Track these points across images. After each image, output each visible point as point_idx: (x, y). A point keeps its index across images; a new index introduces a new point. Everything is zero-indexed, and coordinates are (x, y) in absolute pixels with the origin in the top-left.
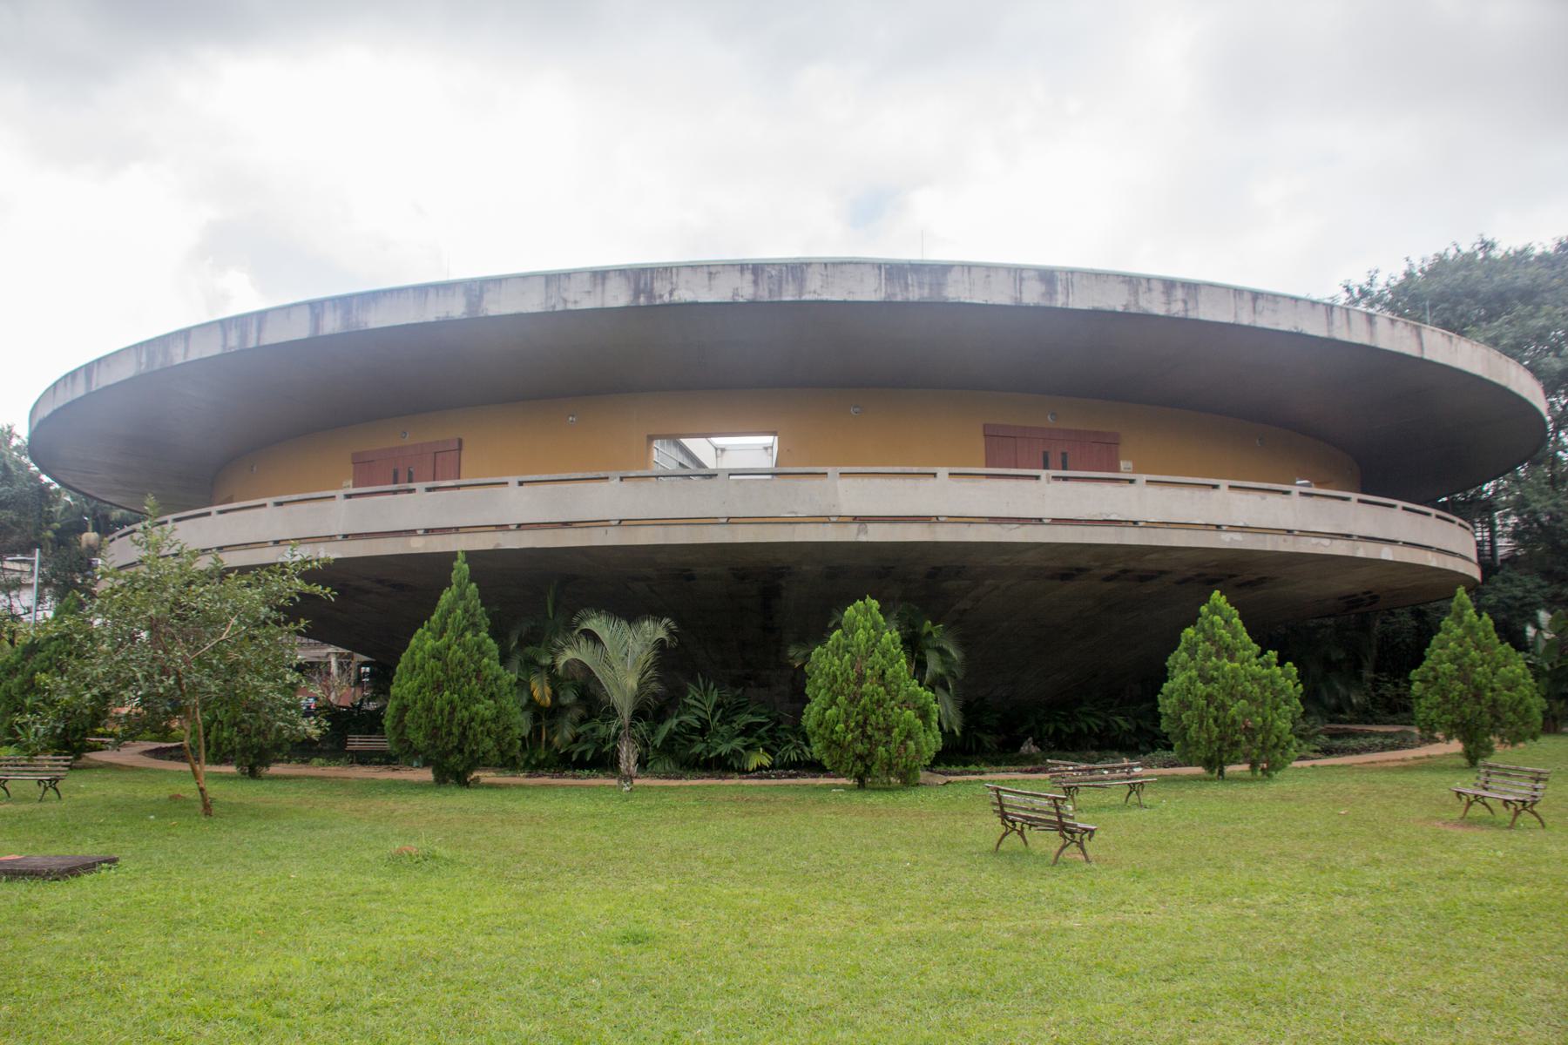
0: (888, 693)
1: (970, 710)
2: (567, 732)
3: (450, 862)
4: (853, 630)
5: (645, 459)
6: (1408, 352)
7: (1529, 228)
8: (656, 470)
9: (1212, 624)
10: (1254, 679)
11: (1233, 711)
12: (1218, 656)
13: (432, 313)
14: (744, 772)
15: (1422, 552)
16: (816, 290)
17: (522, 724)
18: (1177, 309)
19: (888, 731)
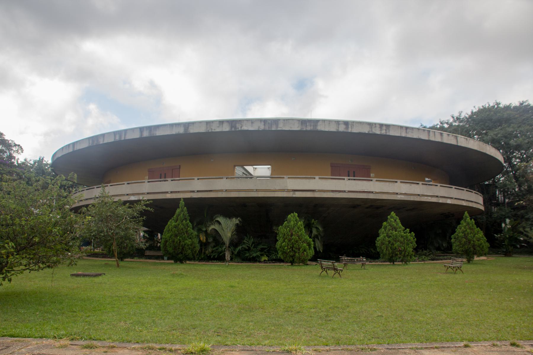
0: (299, 238)
1: (325, 246)
2: (210, 250)
3: (186, 276)
4: (290, 222)
5: (233, 172)
6: (453, 143)
7: (511, 97)
8: (237, 175)
9: (391, 221)
10: (402, 237)
11: (395, 245)
12: (392, 230)
13: (174, 131)
14: (260, 262)
15: (461, 201)
16: (282, 127)
17: (198, 248)
18: (383, 132)
19: (299, 249)
